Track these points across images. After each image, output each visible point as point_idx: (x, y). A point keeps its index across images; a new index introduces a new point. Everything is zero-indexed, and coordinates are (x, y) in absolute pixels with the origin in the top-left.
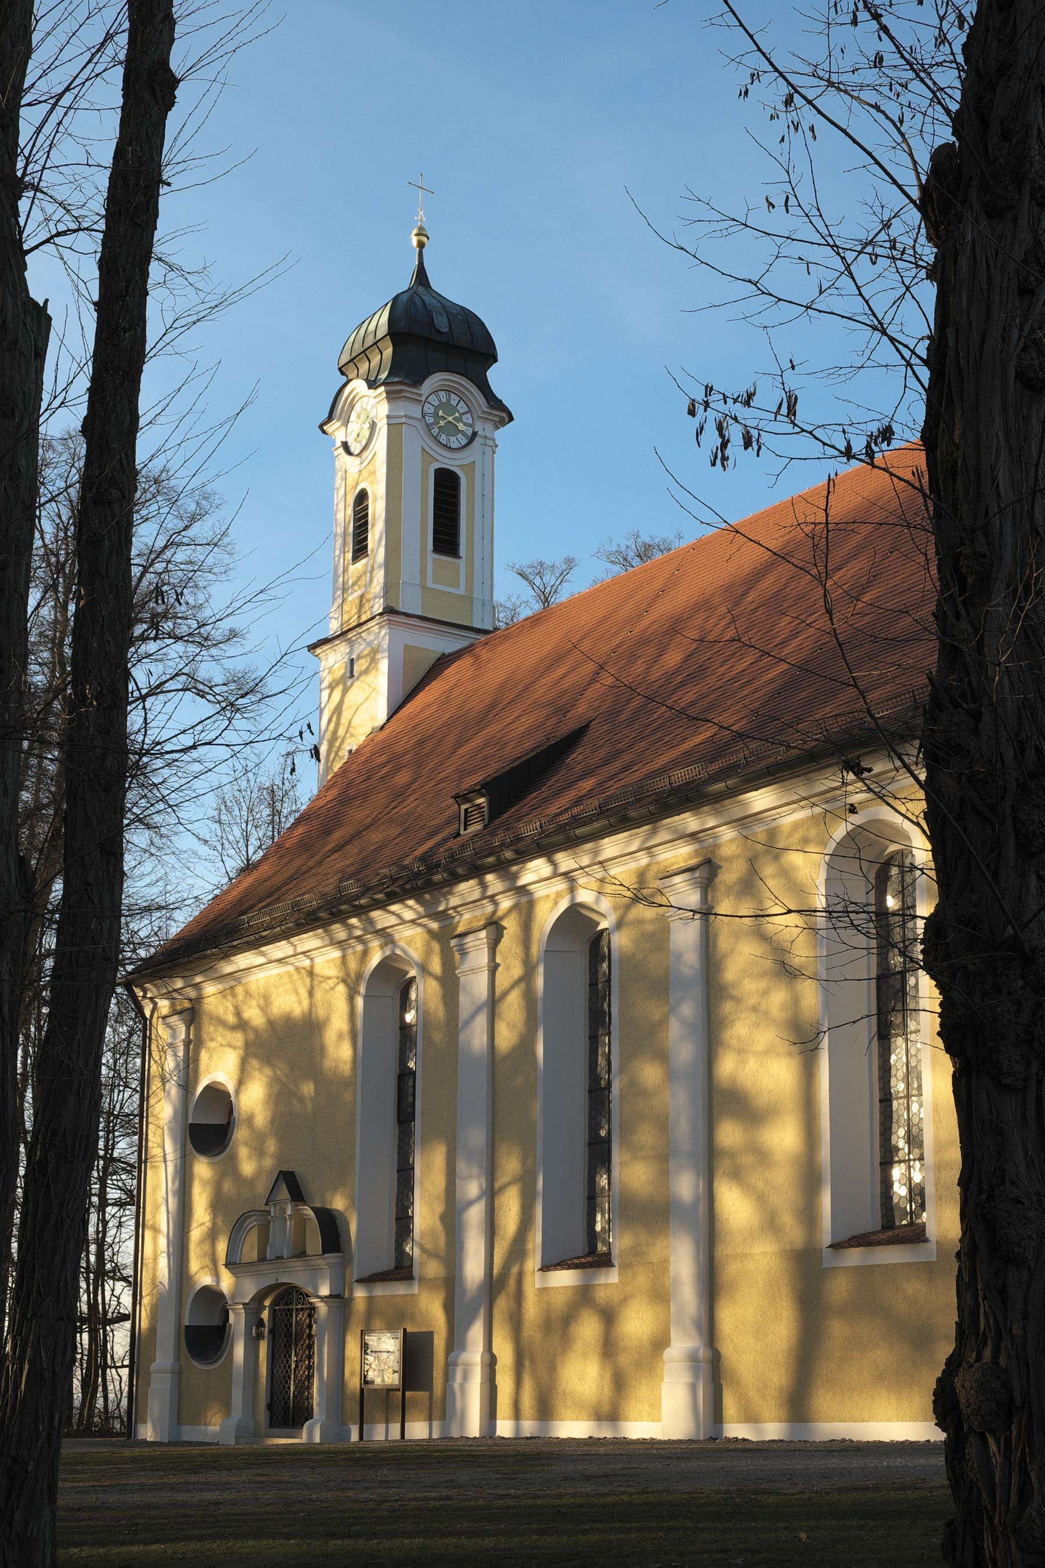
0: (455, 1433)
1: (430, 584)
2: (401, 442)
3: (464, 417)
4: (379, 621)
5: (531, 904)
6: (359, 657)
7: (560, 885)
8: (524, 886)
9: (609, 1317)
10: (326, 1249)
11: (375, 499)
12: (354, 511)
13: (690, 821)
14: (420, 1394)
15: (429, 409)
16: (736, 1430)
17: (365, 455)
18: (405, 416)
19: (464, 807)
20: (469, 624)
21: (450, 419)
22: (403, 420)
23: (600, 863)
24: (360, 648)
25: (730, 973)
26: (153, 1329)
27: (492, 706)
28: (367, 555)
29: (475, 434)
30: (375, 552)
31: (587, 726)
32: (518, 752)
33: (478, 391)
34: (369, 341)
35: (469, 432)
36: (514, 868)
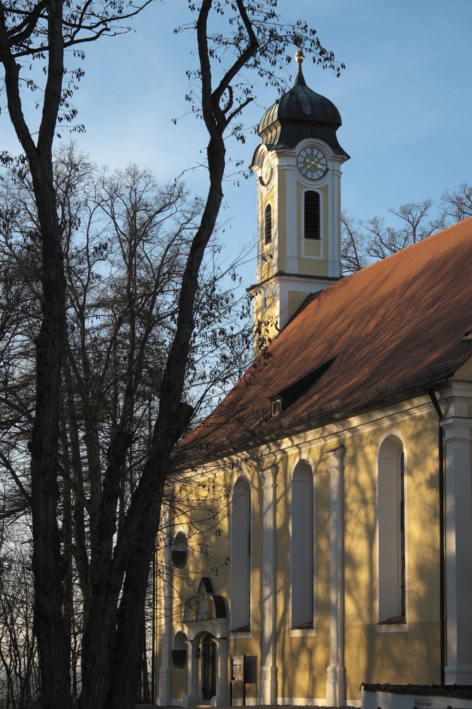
0: (262, 704)
1: (303, 256)
2: (285, 179)
3: (321, 161)
4: (275, 279)
5: (287, 457)
6: (268, 298)
7: (296, 451)
8: (283, 449)
9: (311, 653)
10: (218, 616)
11: (274, 212)
12: (266, 216)
13: (333, 428)
14: (253, 685)
15: (301, 159)
16: (349, 703)
17: (269, 186)
18: (287, 165)
19: (273, 403)
20: (324, 275)
21: (313, 163)
22: (286, 167)
23: (308, 442)
24: (269, 293)
25: (349, 500)
26: (160, 651)
27: (313, 335)
28: (271, 241)
29: (327, 169)
30: (274, 239)
31: (335, 358)
32: (314, 365)
33: (328, 146)
34: (270, 123)
35: (325, 168)
36: (279, 441)
